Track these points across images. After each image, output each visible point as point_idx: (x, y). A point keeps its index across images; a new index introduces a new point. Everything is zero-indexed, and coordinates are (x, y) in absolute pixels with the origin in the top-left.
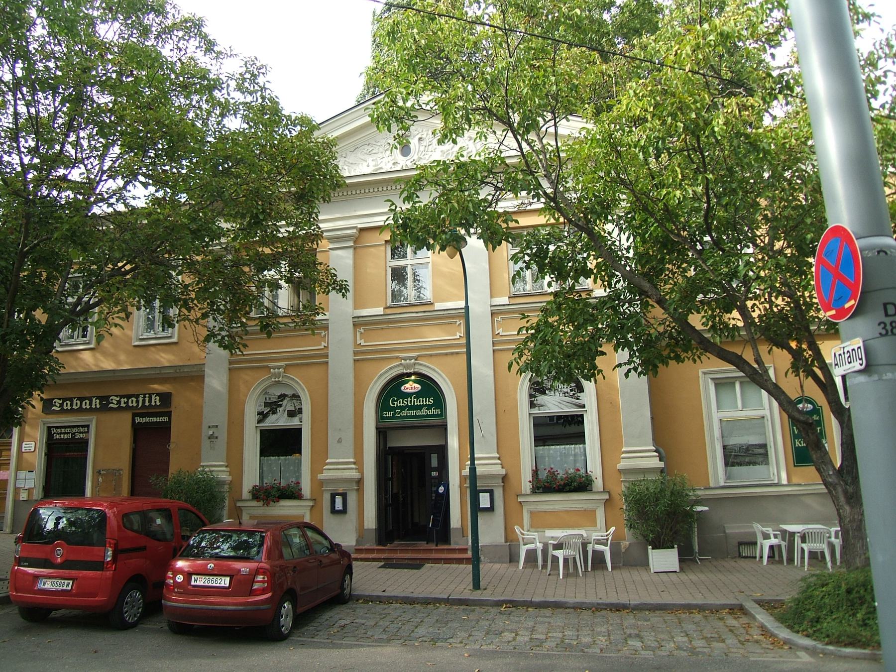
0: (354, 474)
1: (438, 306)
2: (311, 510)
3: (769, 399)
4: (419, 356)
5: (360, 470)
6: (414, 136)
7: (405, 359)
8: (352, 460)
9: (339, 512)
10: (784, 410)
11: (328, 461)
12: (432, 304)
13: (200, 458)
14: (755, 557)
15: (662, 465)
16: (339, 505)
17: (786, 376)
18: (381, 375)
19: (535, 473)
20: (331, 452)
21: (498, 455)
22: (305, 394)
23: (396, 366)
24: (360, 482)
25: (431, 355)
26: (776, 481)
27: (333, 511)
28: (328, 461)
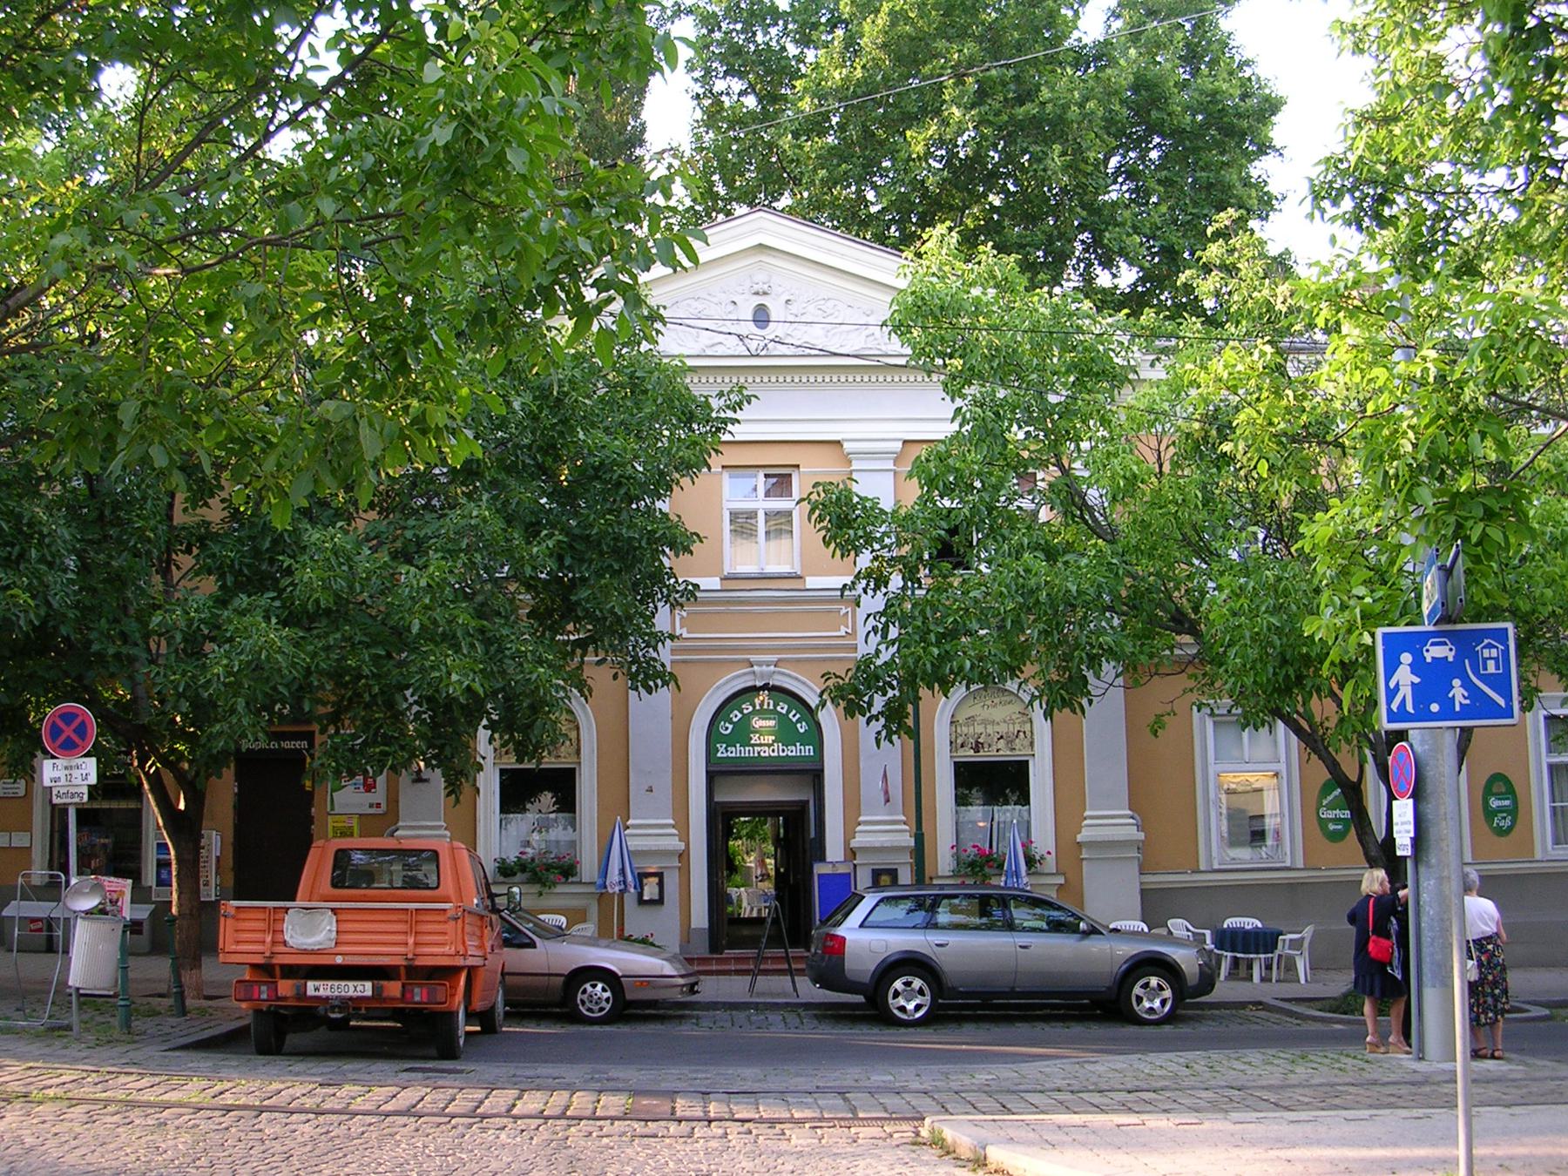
0: (676, 844)
1: (811, 582)
2: (599, 900)
3: (1286, 735)
4: (779, 660)
5: (684, 837)
6: (778, 295)
7: (760, 664)
8: (672, 822)
9: (651, 902)
10: (1315, 750)
11: (861, 819)
12: (800, 577)
13: (1346, 798)
14: (1271, 980)
15: (1141, 836)
16: (650, 891)
17: (878, 747)
18: (718, 688)
19: (957, 846)
20: (1342, 796)
21: (904, 818)
22: (589, 729)
23: (745, 674)
24: (684, 856)
25: (798, 660)
26: (1288, 864)
27: (641, 902)
28: (861, 819)
